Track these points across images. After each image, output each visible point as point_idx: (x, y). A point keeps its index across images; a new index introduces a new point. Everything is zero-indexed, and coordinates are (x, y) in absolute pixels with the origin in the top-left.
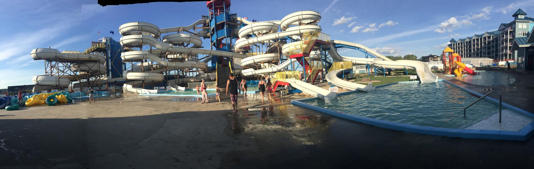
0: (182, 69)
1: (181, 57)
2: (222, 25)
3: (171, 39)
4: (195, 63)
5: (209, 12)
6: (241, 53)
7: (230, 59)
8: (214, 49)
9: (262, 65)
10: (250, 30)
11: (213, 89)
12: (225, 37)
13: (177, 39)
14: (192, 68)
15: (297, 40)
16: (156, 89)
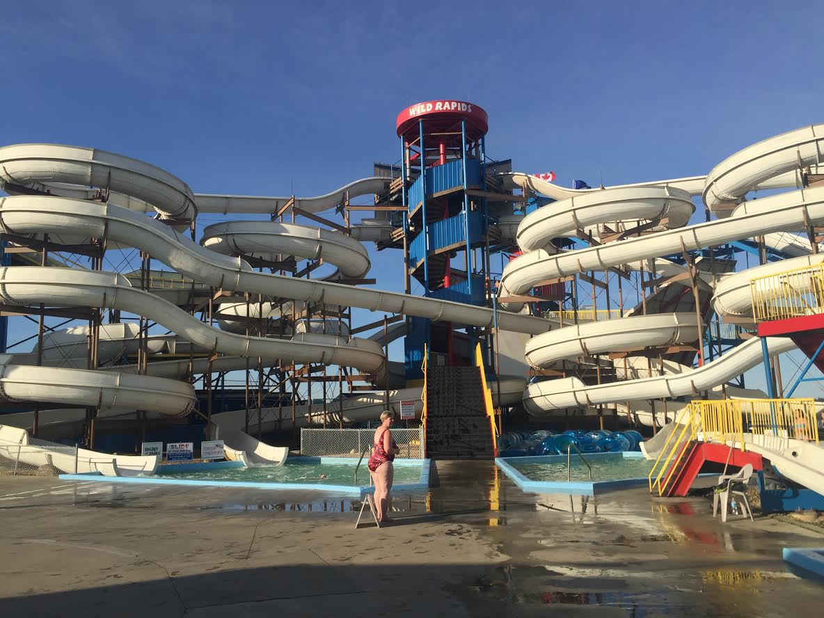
0: (279, 366)
1: (276, 315)
2: (450, 205)
3: (240, 241)
4: (336, 342)
5: (403, 154)
6: (527, 311)
7: (479, 335)
8: (418, 290)
9: (619, 363)
10: (567, 219)
11: (414, 463)
12: (463, 248)
13: (274, 242)
14: (325, 363)
15: (789, 253)
16: (151, 452)
